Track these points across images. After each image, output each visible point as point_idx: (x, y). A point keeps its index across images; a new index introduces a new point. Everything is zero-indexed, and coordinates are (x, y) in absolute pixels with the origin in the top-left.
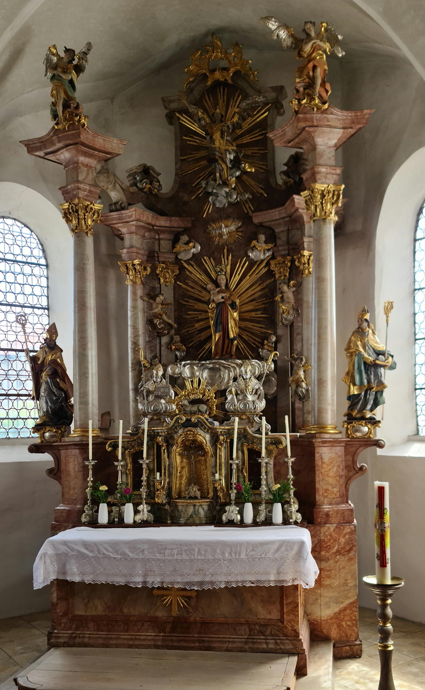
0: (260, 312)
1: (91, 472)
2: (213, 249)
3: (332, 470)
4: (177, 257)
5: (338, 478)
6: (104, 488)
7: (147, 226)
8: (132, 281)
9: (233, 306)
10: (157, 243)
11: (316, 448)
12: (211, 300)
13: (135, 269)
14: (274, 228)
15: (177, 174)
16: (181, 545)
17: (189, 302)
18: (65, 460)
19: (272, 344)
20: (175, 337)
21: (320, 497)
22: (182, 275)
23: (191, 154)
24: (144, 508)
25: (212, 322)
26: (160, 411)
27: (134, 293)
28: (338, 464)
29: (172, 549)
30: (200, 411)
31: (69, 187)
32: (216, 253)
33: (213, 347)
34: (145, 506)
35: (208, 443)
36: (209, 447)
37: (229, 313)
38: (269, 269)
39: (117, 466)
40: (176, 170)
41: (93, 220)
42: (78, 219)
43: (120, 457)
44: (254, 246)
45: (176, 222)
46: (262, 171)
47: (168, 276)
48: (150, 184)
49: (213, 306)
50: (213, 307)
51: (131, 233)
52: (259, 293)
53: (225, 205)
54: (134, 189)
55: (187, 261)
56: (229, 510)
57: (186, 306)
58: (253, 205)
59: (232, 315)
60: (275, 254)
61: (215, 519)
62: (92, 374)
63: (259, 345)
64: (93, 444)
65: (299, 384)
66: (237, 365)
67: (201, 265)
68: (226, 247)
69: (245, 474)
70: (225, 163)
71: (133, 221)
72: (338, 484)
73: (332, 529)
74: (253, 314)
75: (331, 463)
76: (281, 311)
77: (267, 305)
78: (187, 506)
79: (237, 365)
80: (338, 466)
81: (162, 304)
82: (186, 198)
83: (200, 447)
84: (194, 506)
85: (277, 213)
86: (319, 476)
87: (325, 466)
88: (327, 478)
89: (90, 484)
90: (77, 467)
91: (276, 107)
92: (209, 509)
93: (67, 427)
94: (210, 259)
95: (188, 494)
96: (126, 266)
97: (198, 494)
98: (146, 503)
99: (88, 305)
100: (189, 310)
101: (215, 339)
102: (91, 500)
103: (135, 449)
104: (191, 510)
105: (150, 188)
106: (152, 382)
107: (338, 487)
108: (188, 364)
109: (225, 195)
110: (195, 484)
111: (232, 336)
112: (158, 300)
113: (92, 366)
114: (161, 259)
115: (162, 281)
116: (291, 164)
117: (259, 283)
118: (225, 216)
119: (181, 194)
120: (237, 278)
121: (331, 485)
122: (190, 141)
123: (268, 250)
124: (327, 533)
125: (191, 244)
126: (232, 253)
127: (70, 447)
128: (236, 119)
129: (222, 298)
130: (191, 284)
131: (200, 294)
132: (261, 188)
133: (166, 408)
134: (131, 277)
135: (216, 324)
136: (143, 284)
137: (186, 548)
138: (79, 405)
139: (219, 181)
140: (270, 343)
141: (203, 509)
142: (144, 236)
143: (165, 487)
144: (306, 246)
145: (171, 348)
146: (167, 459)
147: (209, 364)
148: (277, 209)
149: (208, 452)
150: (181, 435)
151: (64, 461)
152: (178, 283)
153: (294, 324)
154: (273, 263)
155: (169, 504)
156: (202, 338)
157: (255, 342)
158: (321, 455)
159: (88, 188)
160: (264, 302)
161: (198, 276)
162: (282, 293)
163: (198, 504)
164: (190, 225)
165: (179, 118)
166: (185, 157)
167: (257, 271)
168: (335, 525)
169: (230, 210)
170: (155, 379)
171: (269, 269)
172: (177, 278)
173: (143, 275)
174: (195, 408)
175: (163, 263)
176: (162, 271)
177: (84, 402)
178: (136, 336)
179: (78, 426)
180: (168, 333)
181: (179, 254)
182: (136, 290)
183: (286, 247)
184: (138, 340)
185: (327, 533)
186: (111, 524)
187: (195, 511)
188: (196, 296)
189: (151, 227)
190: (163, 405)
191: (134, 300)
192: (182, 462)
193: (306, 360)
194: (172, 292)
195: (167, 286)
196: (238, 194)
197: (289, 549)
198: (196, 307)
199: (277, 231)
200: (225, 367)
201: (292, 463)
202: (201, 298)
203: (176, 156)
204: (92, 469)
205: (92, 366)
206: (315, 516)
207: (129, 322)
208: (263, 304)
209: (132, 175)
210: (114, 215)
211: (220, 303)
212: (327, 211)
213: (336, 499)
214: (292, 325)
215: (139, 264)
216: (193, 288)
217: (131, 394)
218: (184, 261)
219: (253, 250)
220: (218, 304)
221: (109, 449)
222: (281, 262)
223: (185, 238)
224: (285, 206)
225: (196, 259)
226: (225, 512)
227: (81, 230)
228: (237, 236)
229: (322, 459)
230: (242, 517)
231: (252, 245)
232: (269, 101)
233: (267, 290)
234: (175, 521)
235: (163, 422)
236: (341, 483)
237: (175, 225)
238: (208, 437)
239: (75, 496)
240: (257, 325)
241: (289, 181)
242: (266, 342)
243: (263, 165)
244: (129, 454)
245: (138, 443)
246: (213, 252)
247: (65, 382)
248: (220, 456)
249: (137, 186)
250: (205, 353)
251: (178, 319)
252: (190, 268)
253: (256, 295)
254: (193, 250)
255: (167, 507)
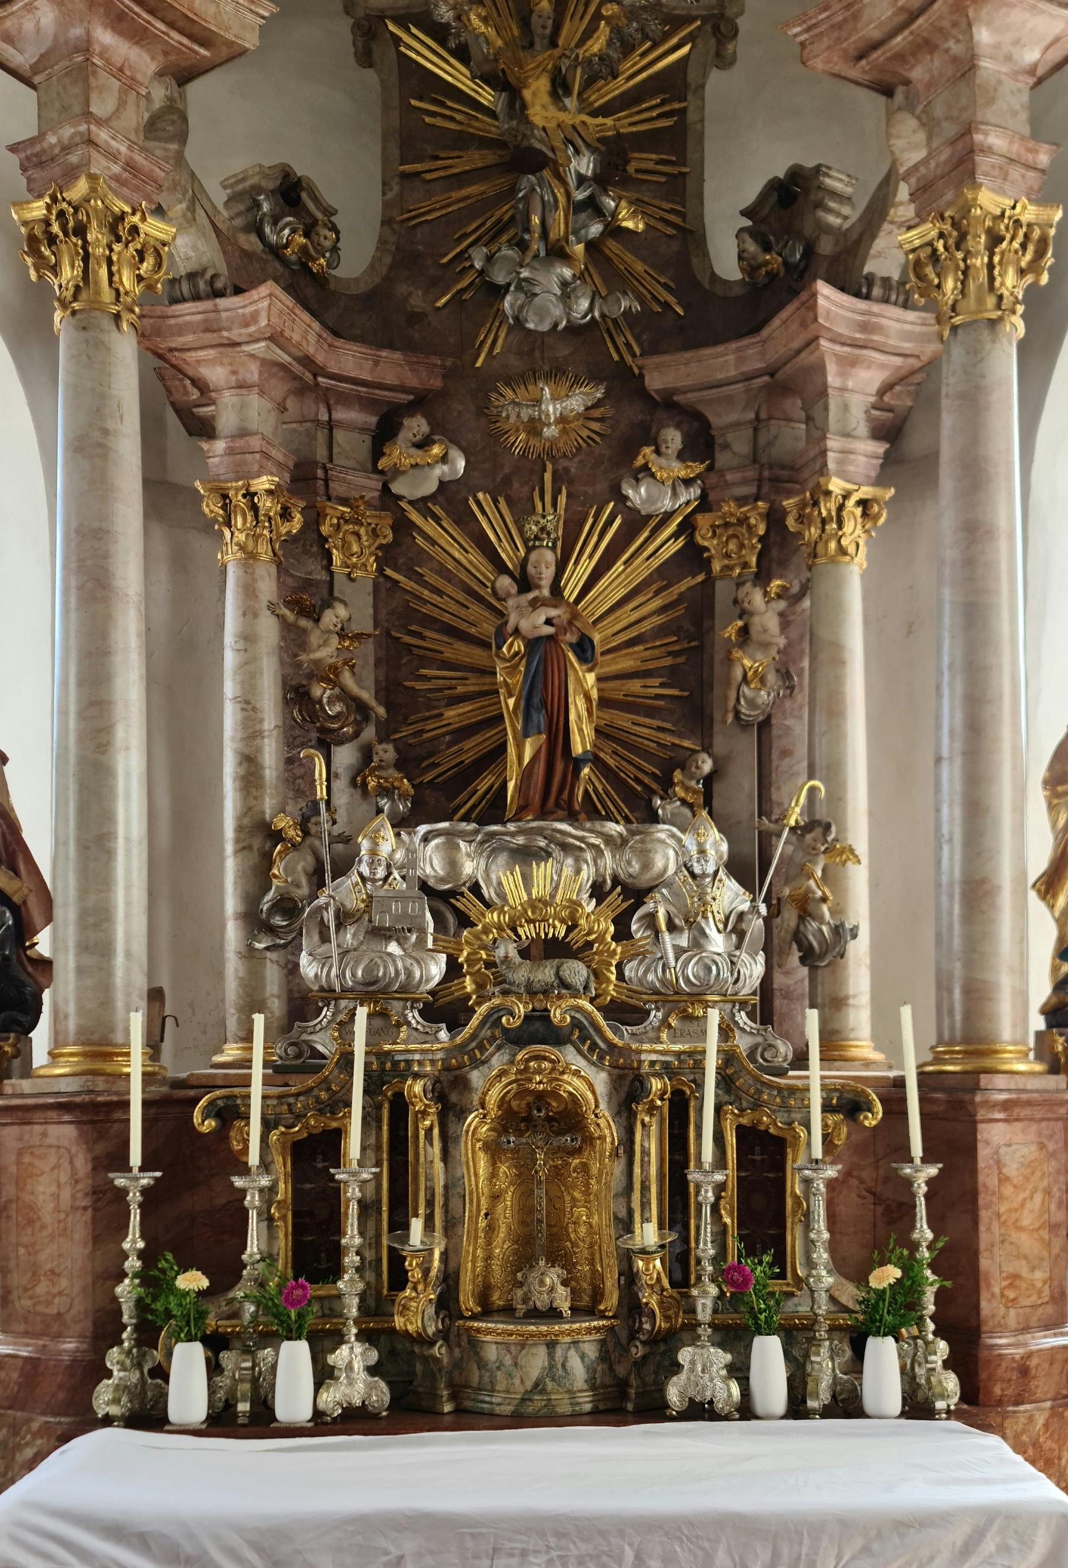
0: (656, 682)
1: (135, 1217)
2: (507, 470)
3: (1029, 1205)
4: (386, 489)
5: (1045, 1234)
6: (193, 1281)
7: (297, 369)
8: (242, 548)
9: (584, 651)
10: (321, 436)
11: (981, 1127)
12: (510, 628)
13: (255, 508)
14: (709, 415)
15: (387, 222)
16: (560, 1535)
17: (423, 638)
18: (19, 1163)
19: (698, 782)
20: (379, 748)
21: (995, 1303)
22: (399, 550)
23: (436, 158)
24: (352, 1356)
25: (511, 702)
26: (389, 985)
27: (249, 591)
28: (1045, 1183)
29: (524, 1553)
30: (564, 984)
31: (52, 139)
32: (516, 485)
33: (511, 785)
34: (358, 1348)
35: (603, 1106)
36: (606, 1126)
37: (570, 672)
38: (691, 544)
39: (243, 1192)
40: (386, 205)
41: (140, 278)
42: (86, 259)
43: (254, 1158)
44: (645, 468)
45: (392, 369)
46: (670, 231)
47: (355, 548)
48: (306, 235)
49: (515, 648)
50: (517, 654)
51: (242, 386)
52: (657, 620)
53: (556, 325)
54: (250, 242)
55: (422, 504)
56: (693, 1363)
57: (415, 651)
58: (637, 339)
59: (579, 682)
60: (712, 496)
61: (631, 1394)
62: (128, 840)
63: (654, 786)
64: (146, 1104)
65: (811, 907)
66: (609, 840)
67: (464, 519)
68: (549, 467)
69: (727, 1220)
70: (563, 181)
71: (257, 341)
72: (1045, 1254)
73: (1040, 1420)
74: (635, 686)
75: (1027, 1179)
76: (738, 673)
77: (681, 660)
78: (523, 1346)
79: (609, 840)
80: (1048, 1192)
81: (342, 635)
82: (417, 301)
83: (568, 1120)
84: (551, 1345)
85: (731, 357)
86: (989, 1229)
87: (1008, 1190)
88: (1015, 1236)
89: (133, 1264)
90: (66, 1194)
91: (716, 29)
92: (604, 1356)
93: (23, 1037)
94: (496, 502)
95: (525, 1300)
96: (225, 497)
97: (563, 1300)
98: (362, 1336)
99: (118, 583)
100: (424, 661)
101: (520, 758)
102: (137, 1328)
103: (306, 1126)
104: (536, 1361)
105: (304, 249)
106: (356, 878)
107: (1046, 1264)
108: (438, 833)
109: (558, 292)
110: (552, 1261)
111: (578, 749)
112: (330, 618)
113: (127, 810)
114: (337, 488)
115: (337, 557)
116: (766, 211)
117: (654, 587)
118: (546, 368)
119: (402, 289)
120: (583, 569)
121: (1026, 1258)
122: (434, 114)
123: (688, 482)
124: (1025, 1438)
125: (436, 450)
126: (570, 483)
127: (38, 1116)
128: (597, 45)
129: (549, 622)
130: (431, 578)
131: (462, 613)
132: (665, 286)
133: (409, 974)
134: (241, 537)
135: (528, 708)
136: (279, 565)
137: (584, 1548)
138: (78, 955)
139: (537, 246)
140: (691, 778)
141: (583, 1357)
142: (282, 408)
143: (434, 1273)
144: (831, 465)
145: (365, 784)
146: (439, 1166)
147: (513, 835)
148: (733, 345)
149: (602, 1138)
150: (502, 1073)
151: (13, 1169)
152: (389, 572)
153: (773, 721)
154: (703, 521)
155: (446, 1339)
156: (468, 758)
157: (641, 776)
158: (997, 1153)
159: (123, 149)
160: (671, 648)
161: (457, 555)
162: (743, 614)
163: (568, 1339)
164: (437, 383)
165: (397, 40)
166: (418, 167)
167: (651, 549)
168: (1048, 1404)
169: (563, 351)
170: (365, 870)
171: (691, 544)
172: (387, 556)
173: (279, 535)
174: (545, 974)
175: (345, 501)
176: (338, 527)
177: (96, 944)
178: (251, 734)
179: (71, 1037)
180: (356, 735)
181: (394, 479)
182: (255, 580)
183: (751, 473)
184: (259, 750)
185: (1025, 1438)
186: (221, 1422)
187: (552, 1366)
188: (446, 618)
189: (308, 377)
190: (400, 965)
191: (248, 613)
192: (493, 1175)
193: (837, 832)
194: (370, 599)
195: (353, 580)
196: (595, 295)
197: (1013, 1543)
198: (448, 654)
199: (715, 421)
200: (565, 847)
201: (929, 1182)
202: (464, 626)
203: (385, 161)
204: (140, 1206)
205: (127, 810)
206: (984, 1375)
207: (230, 688)
208: (670, 654)
209: (245, 197)
210: (190, 312)
211: (539, 639)
212: (1006, 293)
213: (1040, 1311)
214: (765, 725)
215: (270, 492)
216: (440, 593)
217: (233, 933)
218: (411, 503)
219: (638, 480)
220: (533, 644)
221: (208, 1125)
222: (734, 520)
223: (416, 426)
224: (765, 332)
225: (451, 498)
226: (677, 1368)
227: (96, 305)
228: (585, 433)
229: (999, 1164)
230: (746, 1392)
231: (640, 461)
232: (695, 13)
233: (680, 611)
234: (468, 1404)
235: (398, 1025)
236: (1055, 1250)
237: (390, 378)
238: (601, 1080)
239: (59, 1304)
240: (648, 721)
241: (767, 263)
242: (678, 776)
243: (672, 211)
244: (284, 1148)
245: (317, 1099)
246: (507, 481)
247: (17, 873)
248: (645, 1153)
249: (261, 236)
250: (475, 806)
251: (390, 691)
252: (429, 527)
253: (646, 626)
254: (440, 471)
255: (439, 1350)
